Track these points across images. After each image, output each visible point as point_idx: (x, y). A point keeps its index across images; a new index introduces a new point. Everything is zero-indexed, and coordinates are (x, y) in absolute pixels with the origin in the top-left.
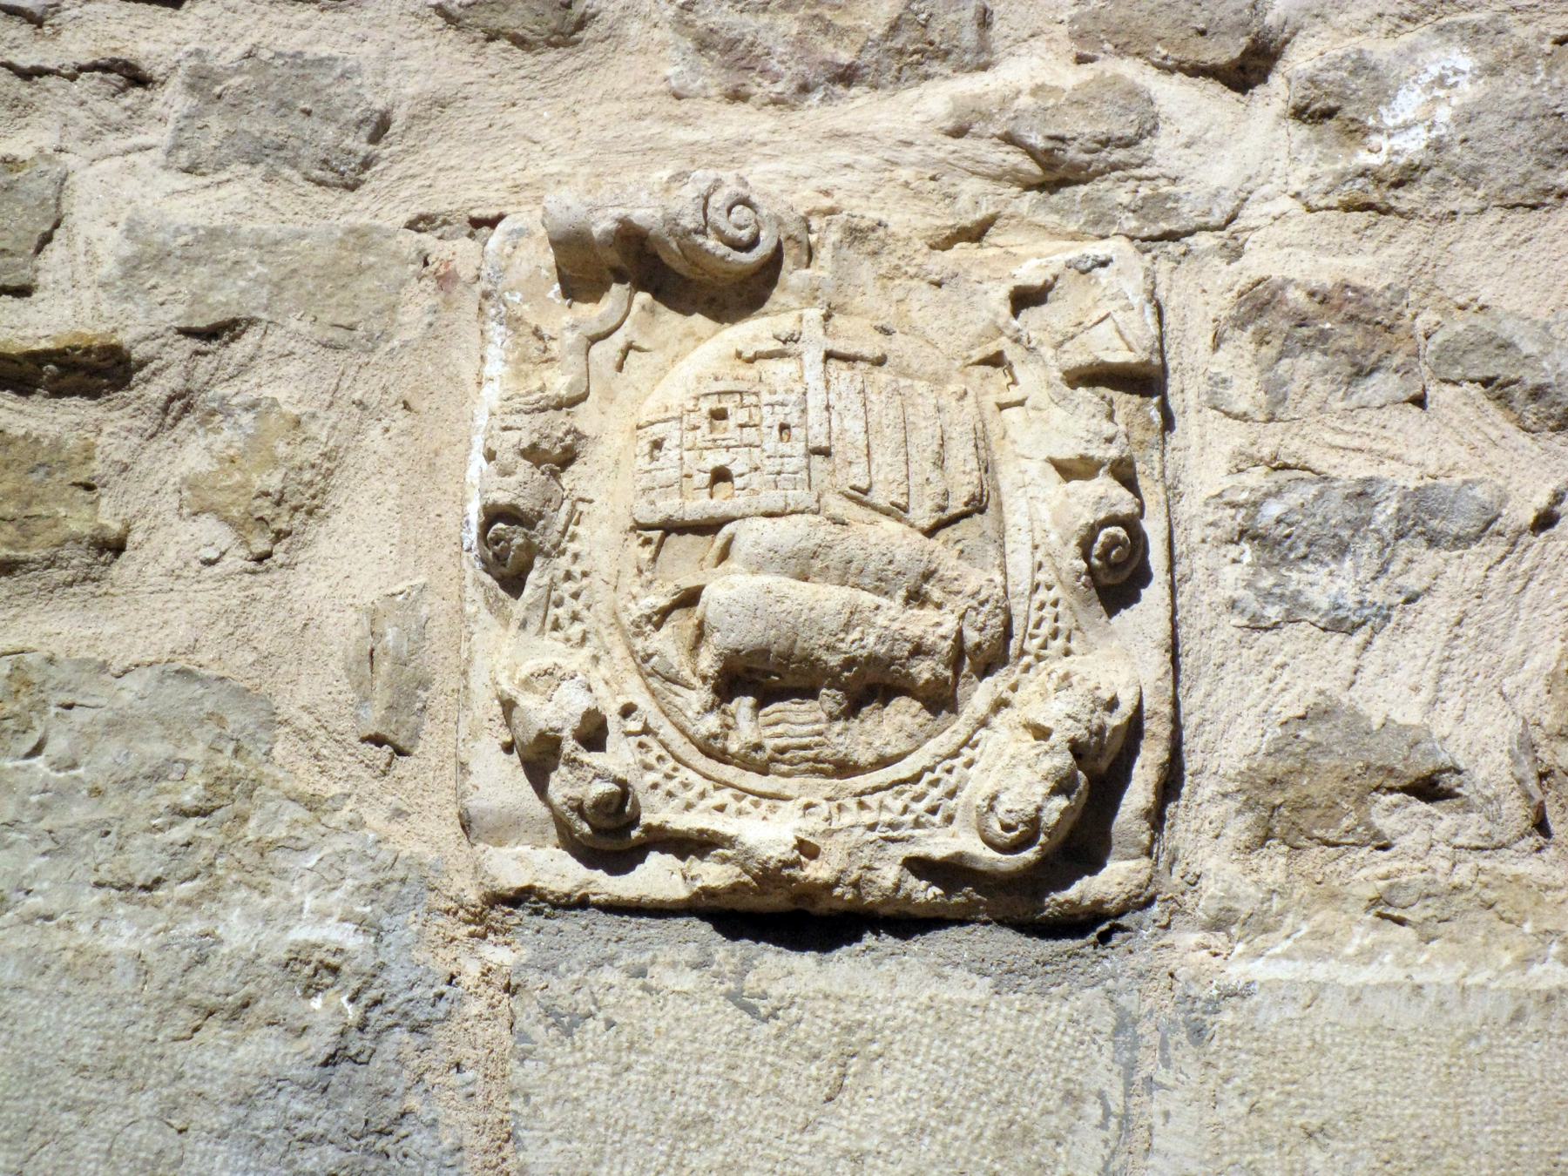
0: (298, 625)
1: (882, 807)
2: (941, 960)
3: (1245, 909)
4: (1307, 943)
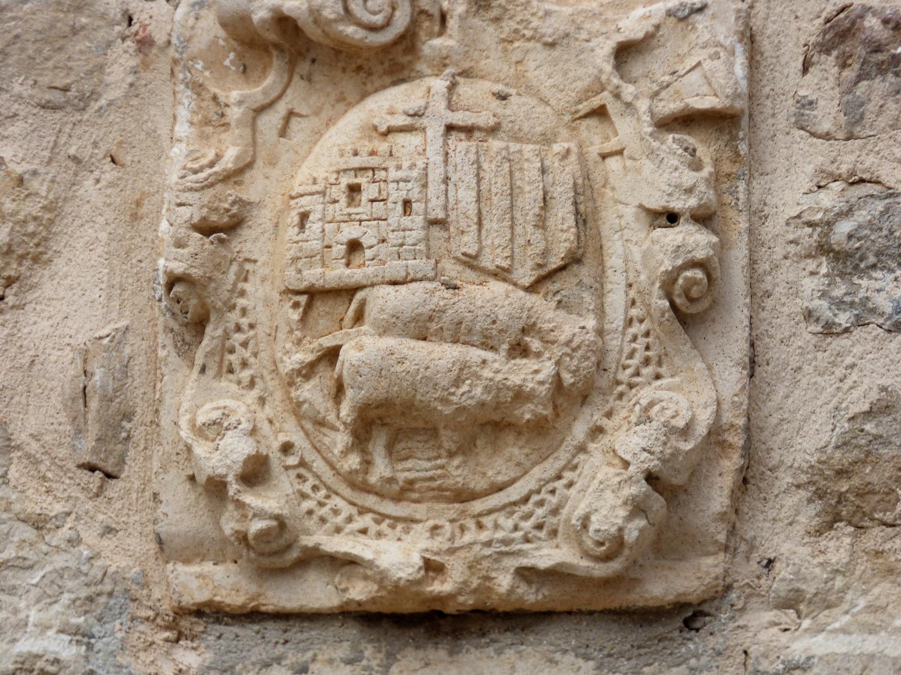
0: (26, 361)
1: (497, 526)
2: (552, 648)
3: (810, 589)
4: (863, 618)
